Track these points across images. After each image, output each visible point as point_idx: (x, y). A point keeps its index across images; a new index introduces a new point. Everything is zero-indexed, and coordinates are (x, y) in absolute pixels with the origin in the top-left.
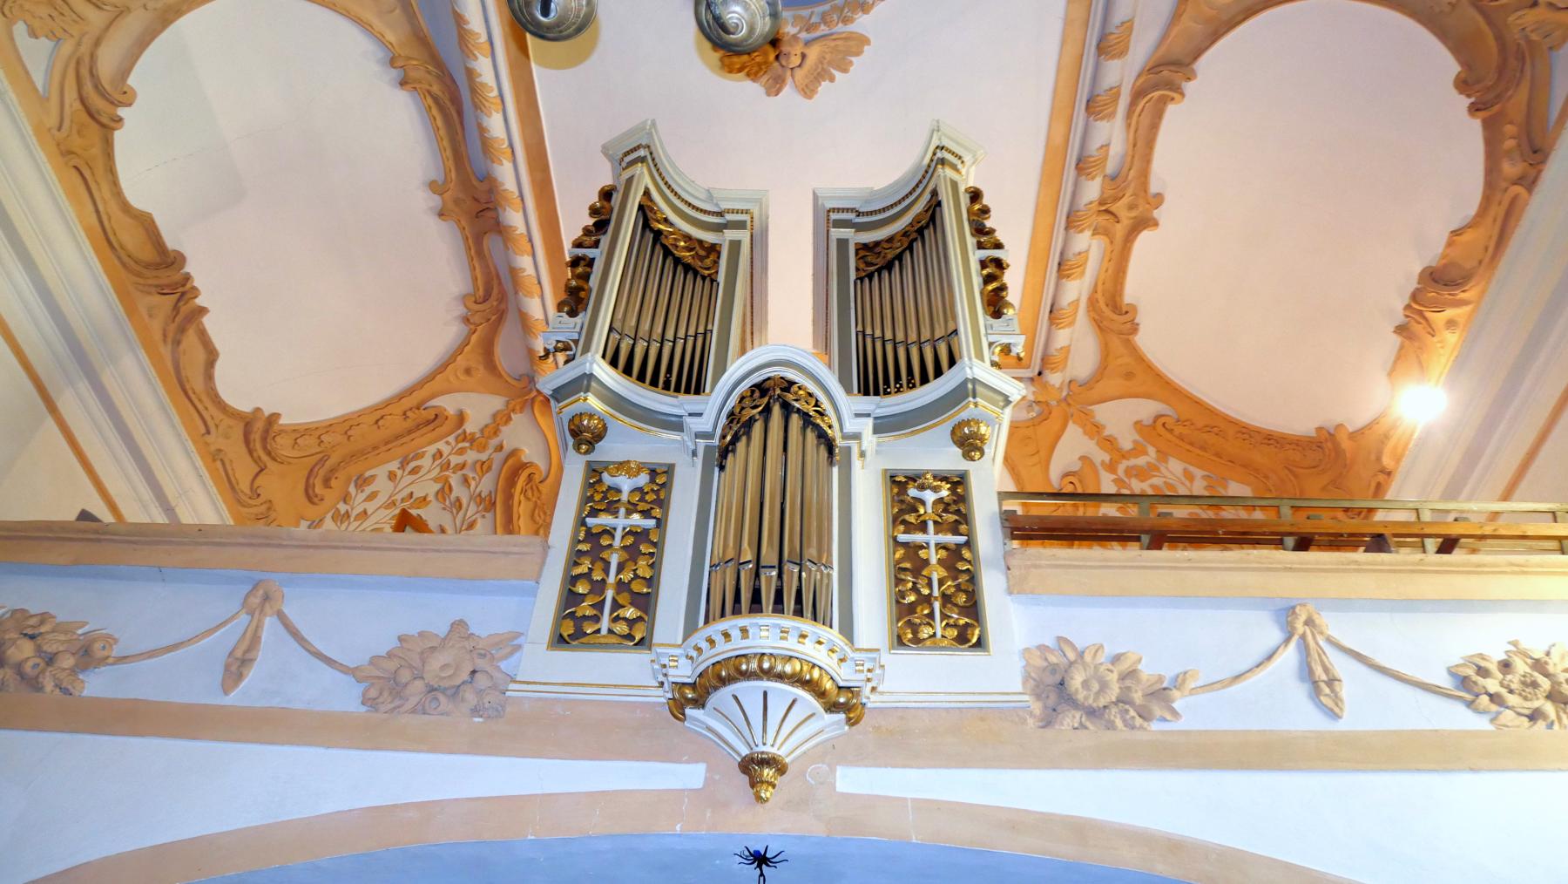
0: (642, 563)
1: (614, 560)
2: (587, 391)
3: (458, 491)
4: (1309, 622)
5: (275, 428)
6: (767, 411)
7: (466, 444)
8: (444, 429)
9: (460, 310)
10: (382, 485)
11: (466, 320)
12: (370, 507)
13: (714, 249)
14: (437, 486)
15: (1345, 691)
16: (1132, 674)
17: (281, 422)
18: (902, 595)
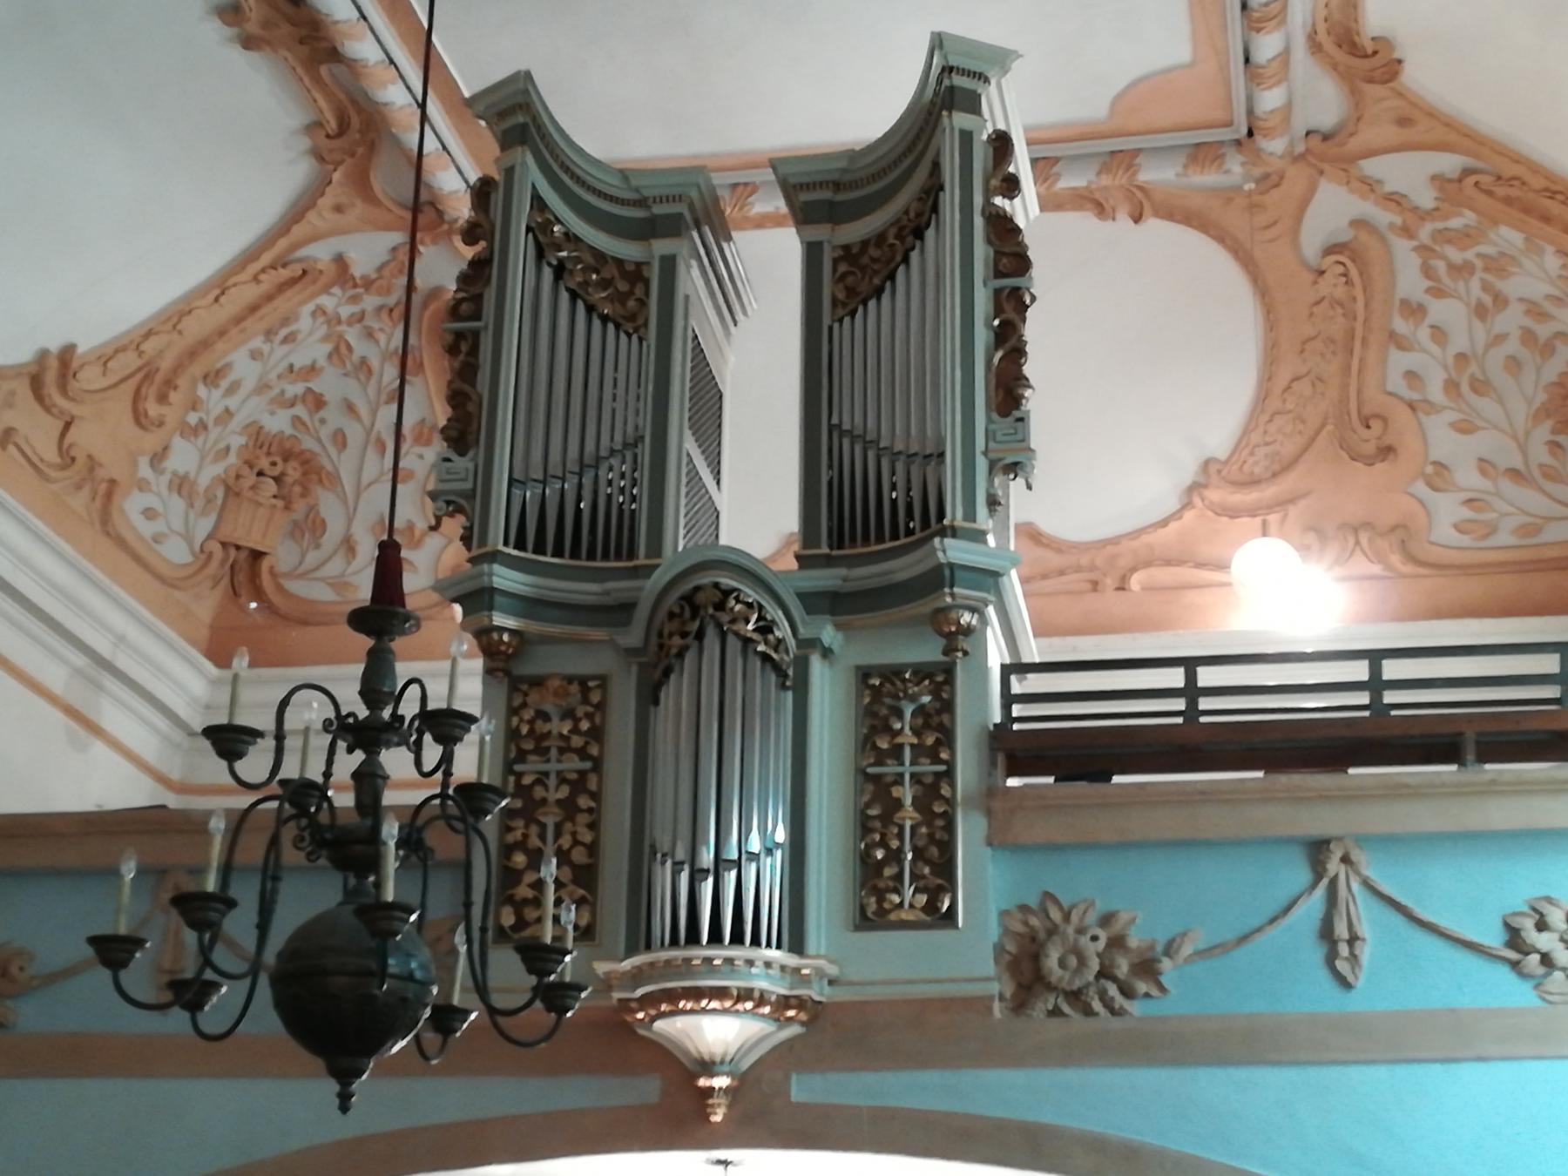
0: (583, 819)
1: (550, 822)
2: (491, 608)
3: (360, 348)
4: (1346, 859)
5: (75, 364)
6: (700, 636)
7: (360, 290)
8: (319, 285)
9: (305, 143)
10: (244, 368)
11: (318, 155)
12: (232, 403)
13: (636, 274)
14: (328, 347)
15: (1366, 953)
16: (1117, 943)
17: (81, 350)
18: (870, 847)
